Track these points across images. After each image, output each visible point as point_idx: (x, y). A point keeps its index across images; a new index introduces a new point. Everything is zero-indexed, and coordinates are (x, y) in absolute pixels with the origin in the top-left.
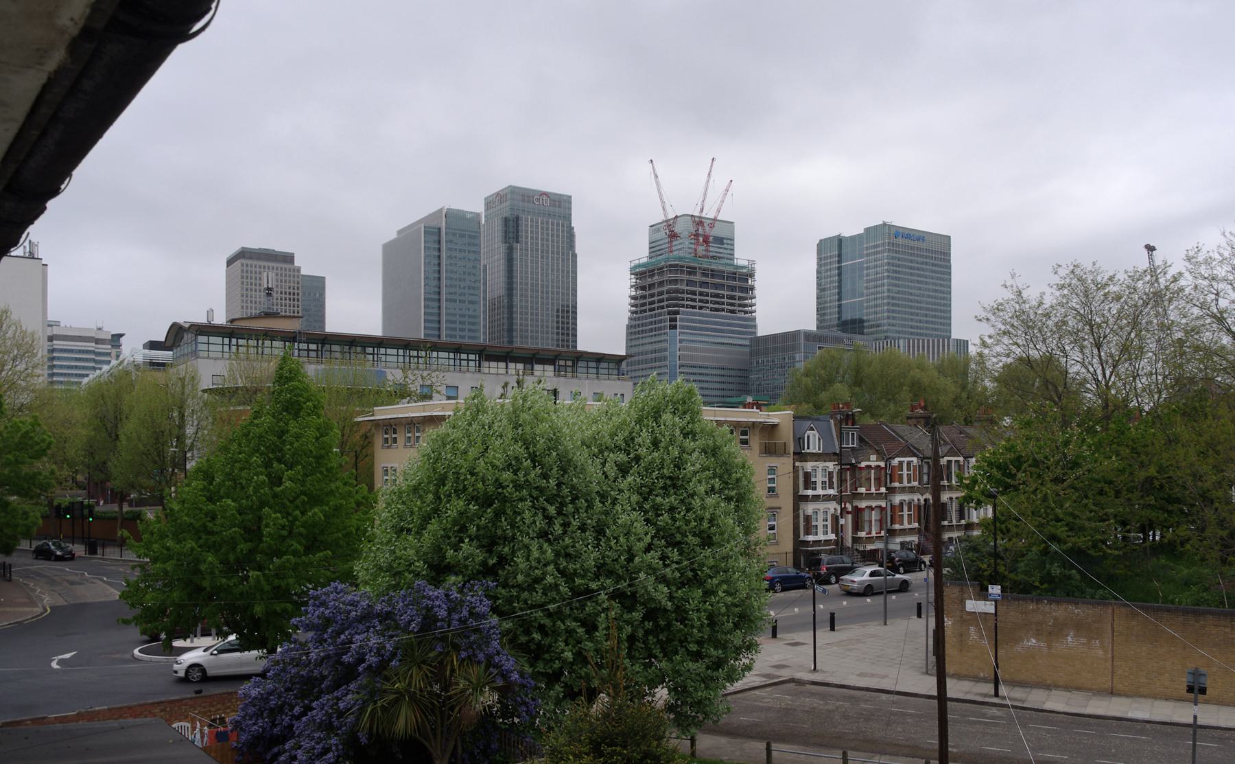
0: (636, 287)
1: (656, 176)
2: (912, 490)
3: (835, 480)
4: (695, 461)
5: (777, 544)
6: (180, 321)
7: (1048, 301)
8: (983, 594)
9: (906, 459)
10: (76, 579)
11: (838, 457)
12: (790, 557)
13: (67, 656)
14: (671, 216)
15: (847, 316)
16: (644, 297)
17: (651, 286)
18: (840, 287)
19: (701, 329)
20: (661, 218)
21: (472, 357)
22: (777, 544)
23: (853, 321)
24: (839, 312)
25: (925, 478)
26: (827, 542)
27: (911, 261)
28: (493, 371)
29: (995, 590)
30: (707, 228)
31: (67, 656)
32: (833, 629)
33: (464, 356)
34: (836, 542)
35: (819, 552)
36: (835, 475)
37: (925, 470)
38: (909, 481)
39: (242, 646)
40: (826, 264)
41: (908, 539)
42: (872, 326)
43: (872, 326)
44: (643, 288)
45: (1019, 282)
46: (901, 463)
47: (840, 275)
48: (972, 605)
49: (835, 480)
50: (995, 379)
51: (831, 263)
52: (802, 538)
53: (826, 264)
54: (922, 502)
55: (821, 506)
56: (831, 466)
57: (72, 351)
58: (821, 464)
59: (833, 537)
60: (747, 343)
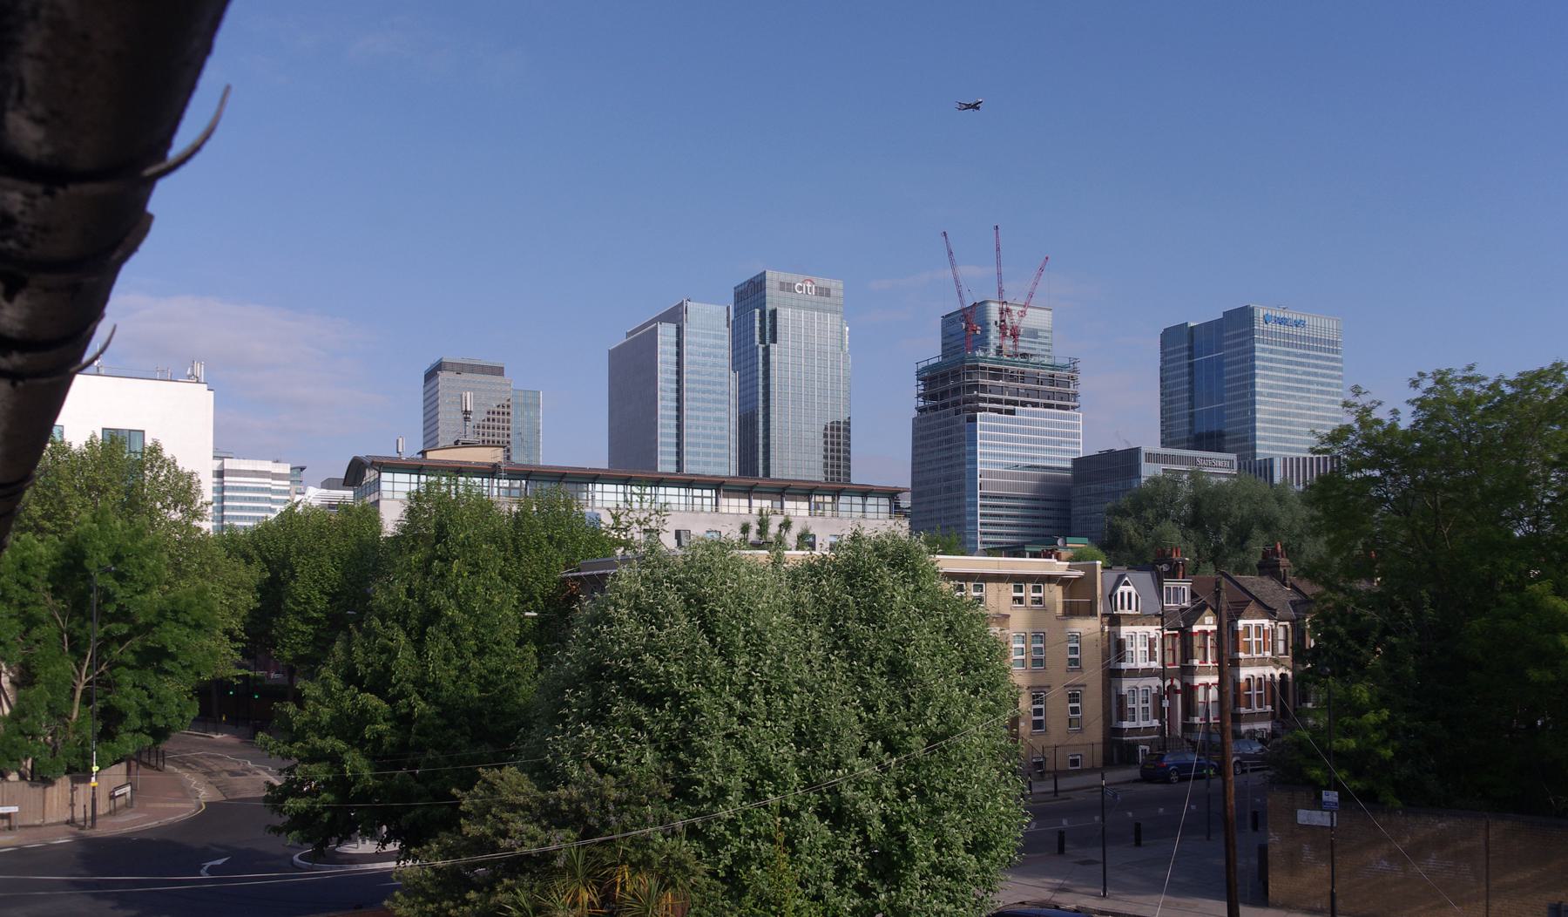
0: (925, 397)
1: (951, 253)
2: (1262, 662)
3: (1157, 649)
4: (924, 635)
5: (1081, 731)
6: (362, 454)
7: (1405, 423)
8: (1318, 804)
9: (1254, 622)
10: (237, 768)
11: (1162, 617)
12: (1099, 749)
13: (219, 862)
14: (968, 304)
15: (1202, 427)
16: (934, 408)
17: (944, 394)
18: (1191, 390)
19: (1044, 442)
20: (957, 307)
21: (707, 493)
22: (1081, 731)
23: (1210, 435)
24: (1191, 423)
25: (1281, 646)
26: (1148, 730)
27: (1288, 354)
28: (733, 510)
29: (1331, 796)
30: (1016, 318)
31: (219, 862)
32: (1138, 843)
33: (697, 492)
34: (1161, 730)
35: (1135, 744)
36: (1158, 643)
37: (1281, 636)
38: (1259, 651)
39: (404, 854)
40: (1173, 361)
41: (1257, 726)
42: (1236, 440)
43: (1236, 440)
44: (933, 397)
45: (1363, 400)
46: (1247, 628)
47: (1191, 374)
48: (1304, 816)
49: (1157, 649)
50: (1316, 533)
51: (1180, 359)
52: (1114, 724)
53: (1173, 361)
54: (1277, 677)
55: (1142, 683)
56: (1153, 631)
57: (245, 489)
58: (1139, 629)
59: (1156, 723)
60: (1069, 465)
